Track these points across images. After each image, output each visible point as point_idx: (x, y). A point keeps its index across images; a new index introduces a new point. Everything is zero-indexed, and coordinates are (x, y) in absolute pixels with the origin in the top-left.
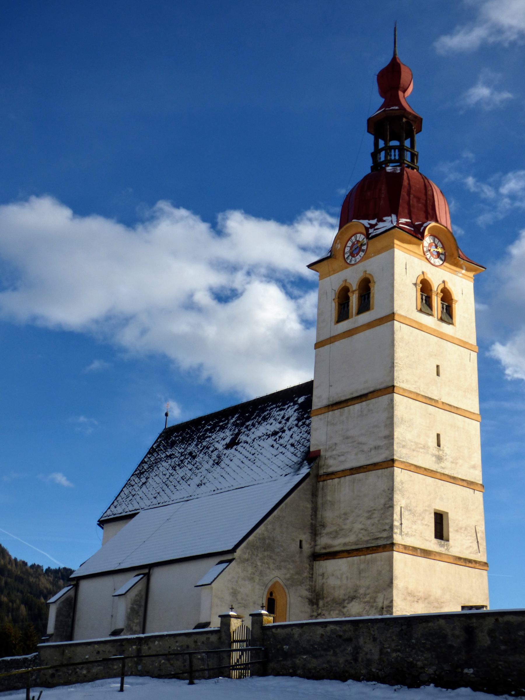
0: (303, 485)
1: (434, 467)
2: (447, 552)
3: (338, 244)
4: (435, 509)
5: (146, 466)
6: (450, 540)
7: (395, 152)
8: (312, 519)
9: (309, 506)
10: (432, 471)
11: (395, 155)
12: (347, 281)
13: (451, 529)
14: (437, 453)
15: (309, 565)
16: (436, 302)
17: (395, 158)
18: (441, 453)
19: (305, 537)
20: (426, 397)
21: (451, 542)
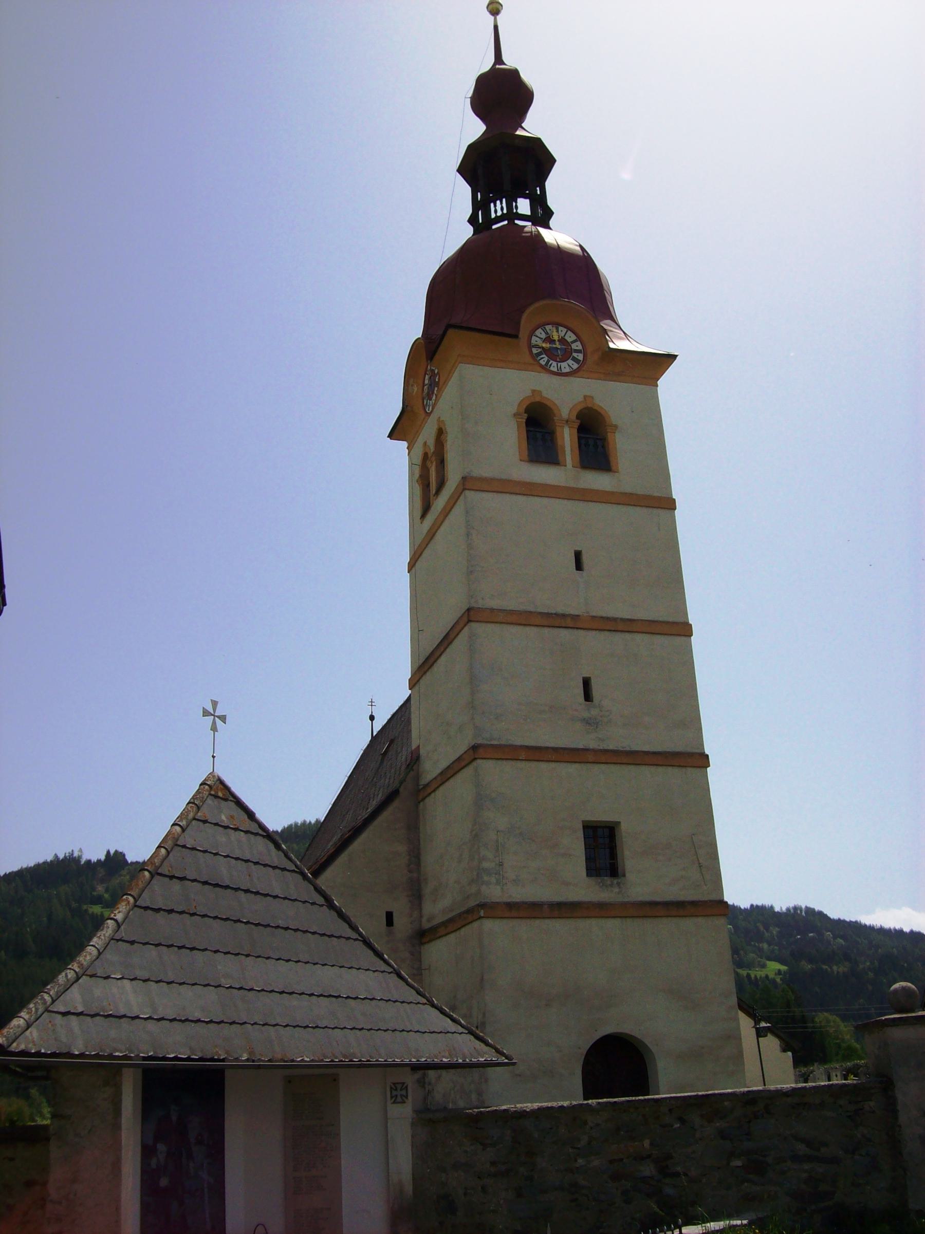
0: (386, 815)
1: (589, 741)
2: (620, 899)
3: (412, 385)
4: (583, 821)
5: (477, 774)
6: (627, 875)
7: (501, 203)
8: (410, 871)
9: (402, 848)
10: (577, 750)
11: (496, 211)
12: (427, 444)
13: (627, 853)
14: (586, 715)
15: (412, 954)
16: (567, 438)
17: (503, 213)
18: (594, 712)
19: (400, 907)
20: (548, 615)
21: (631, 876)
